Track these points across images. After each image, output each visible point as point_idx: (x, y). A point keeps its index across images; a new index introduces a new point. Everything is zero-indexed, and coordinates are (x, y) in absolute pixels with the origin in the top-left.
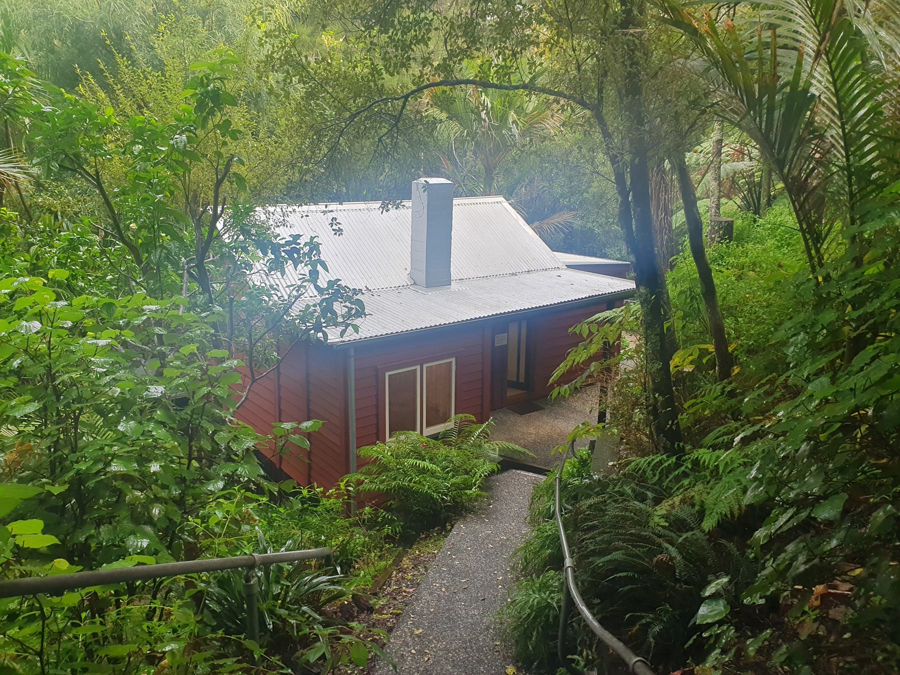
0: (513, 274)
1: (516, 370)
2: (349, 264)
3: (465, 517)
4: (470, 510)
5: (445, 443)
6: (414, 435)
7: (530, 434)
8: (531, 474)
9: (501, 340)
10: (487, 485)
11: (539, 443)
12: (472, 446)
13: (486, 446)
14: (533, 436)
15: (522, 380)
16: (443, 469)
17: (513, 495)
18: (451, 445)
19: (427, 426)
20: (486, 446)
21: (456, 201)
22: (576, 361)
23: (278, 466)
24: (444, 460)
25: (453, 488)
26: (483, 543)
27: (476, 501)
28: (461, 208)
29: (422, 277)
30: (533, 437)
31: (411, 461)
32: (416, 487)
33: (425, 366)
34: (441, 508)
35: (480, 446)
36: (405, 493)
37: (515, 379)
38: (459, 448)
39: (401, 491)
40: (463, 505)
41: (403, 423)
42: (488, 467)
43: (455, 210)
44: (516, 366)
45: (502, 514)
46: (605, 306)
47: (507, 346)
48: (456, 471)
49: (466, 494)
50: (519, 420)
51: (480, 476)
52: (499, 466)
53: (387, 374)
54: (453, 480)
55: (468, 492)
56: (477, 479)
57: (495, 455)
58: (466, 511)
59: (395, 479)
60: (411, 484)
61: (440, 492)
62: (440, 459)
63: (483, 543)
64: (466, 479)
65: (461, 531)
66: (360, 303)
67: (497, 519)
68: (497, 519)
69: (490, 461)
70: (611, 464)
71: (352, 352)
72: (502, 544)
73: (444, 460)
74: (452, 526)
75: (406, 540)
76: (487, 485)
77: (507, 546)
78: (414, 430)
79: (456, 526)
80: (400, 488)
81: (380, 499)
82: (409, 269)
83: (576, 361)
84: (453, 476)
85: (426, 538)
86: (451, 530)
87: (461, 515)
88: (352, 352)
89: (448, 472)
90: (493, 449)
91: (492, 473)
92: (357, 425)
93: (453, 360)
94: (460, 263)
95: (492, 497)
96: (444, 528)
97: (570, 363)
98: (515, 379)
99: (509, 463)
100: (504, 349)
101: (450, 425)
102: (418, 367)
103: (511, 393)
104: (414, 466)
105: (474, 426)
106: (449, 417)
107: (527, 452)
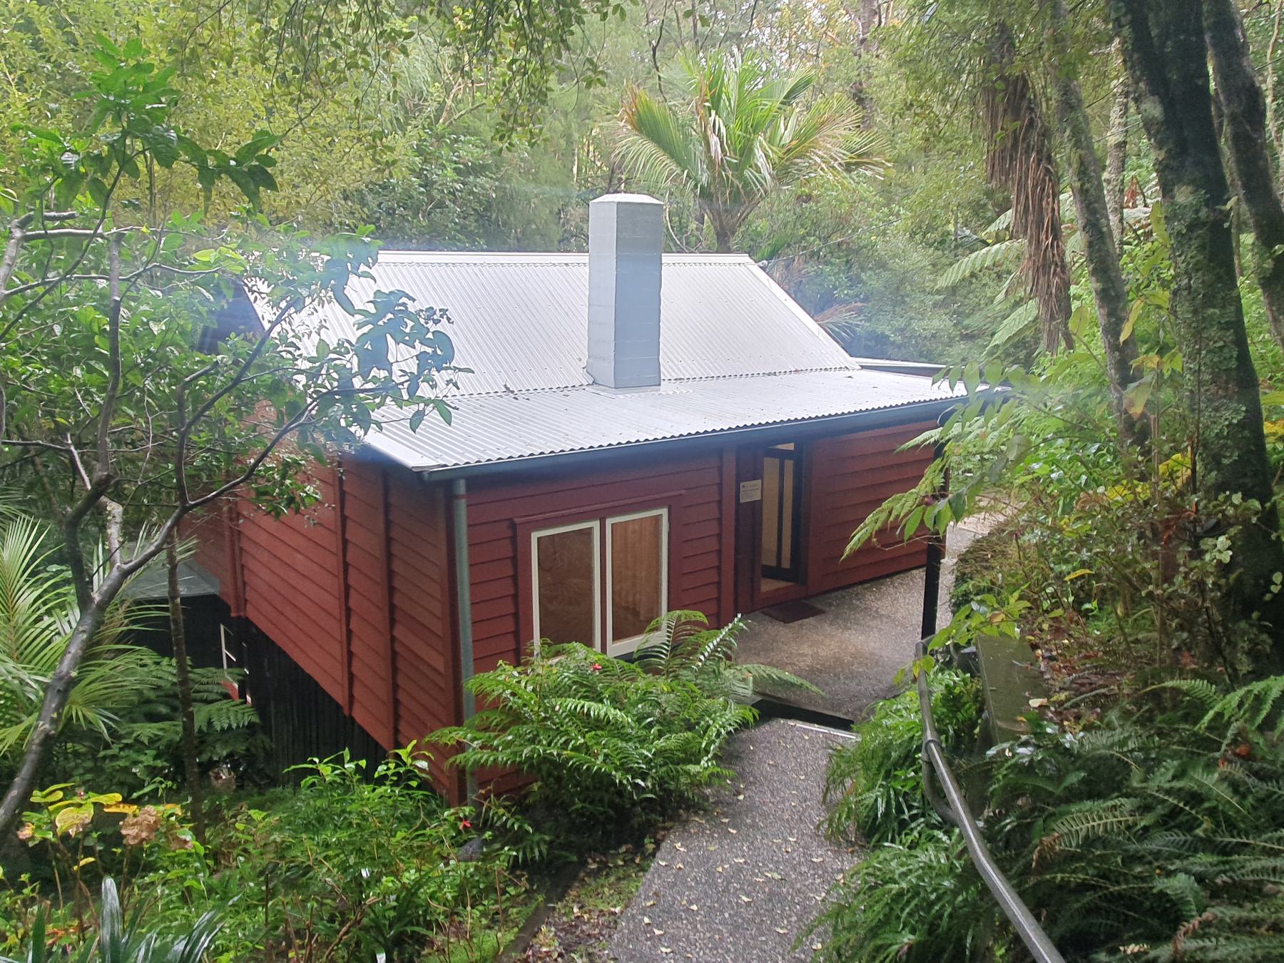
0: (769, 374)
1: (775, 549)
3: (687, 821)
4: (695, 807)
7: (803, 655)
8: (816, 727)
10: (729, 754)
11: (821, 671)
12: (701, 671)
13: (727, 673)
15: (786, 564)
16: (640, 719)
17: (784, 772)
20: (727, 673)
22: (894, 513)
25: (660, 760)
26: (726, 890)
27: (709, 785)
30: (809, 660)
31: (571, 703)
32: (573, 758)
34: (634, 804)
35: (717, 674)
36: (550, 769)
37: (773, 563)
39: (545, 767)
40: (681, 795)
41: (568, 626)
42: (734, 714)
43: (665, 271)
44: (783, 528)
45: (765, 816)
47: (760, 502)
48: (666, 725)
49: (687, 773)
50: (782, 631)
51: (718, 734)
52: (756, 712)
53: (535, 536)
54: (660, 743)
55: (693, 768)
56: (712, 739)
57: (747, 691)
58: (687, 809)
59: (533, 741)
61: (629, 770)
62: (634, 698)
63: (726, 890)
64: (687, 741)
65: (677, 853)
66: (442, 340)
67: (754, 826)
68: (754, 826)
69: (739, 702)
70: (1035, 703)
71: (461, 488)
72: (772, 893)
73: (641, 700)
74: (658, 844)
75: (553, 874)
76: (729, 754)
77: (782, 900)
78: (589, 643)
79: (665, 845)
80: (546, 759)
81: (511, 783)
82: (585, 360)
84: (660, 735)
85: (599, 870)
86: (653, 855)
87: (674, 817)
88: (461, 488)
89: (650, 725)
90: (743, 679)
91: (744, 725)
93: (664, 512)
94: (674, 353)
95: (742, 776)
96: (639, 846)
97: (883, 516)
99: (773, 706)
100: (756, 507)
101: (658, 639)
102: (595, 525)
103: (767, 586)
105: (705, 633)
106: (654, 612)
107: (806, 684)
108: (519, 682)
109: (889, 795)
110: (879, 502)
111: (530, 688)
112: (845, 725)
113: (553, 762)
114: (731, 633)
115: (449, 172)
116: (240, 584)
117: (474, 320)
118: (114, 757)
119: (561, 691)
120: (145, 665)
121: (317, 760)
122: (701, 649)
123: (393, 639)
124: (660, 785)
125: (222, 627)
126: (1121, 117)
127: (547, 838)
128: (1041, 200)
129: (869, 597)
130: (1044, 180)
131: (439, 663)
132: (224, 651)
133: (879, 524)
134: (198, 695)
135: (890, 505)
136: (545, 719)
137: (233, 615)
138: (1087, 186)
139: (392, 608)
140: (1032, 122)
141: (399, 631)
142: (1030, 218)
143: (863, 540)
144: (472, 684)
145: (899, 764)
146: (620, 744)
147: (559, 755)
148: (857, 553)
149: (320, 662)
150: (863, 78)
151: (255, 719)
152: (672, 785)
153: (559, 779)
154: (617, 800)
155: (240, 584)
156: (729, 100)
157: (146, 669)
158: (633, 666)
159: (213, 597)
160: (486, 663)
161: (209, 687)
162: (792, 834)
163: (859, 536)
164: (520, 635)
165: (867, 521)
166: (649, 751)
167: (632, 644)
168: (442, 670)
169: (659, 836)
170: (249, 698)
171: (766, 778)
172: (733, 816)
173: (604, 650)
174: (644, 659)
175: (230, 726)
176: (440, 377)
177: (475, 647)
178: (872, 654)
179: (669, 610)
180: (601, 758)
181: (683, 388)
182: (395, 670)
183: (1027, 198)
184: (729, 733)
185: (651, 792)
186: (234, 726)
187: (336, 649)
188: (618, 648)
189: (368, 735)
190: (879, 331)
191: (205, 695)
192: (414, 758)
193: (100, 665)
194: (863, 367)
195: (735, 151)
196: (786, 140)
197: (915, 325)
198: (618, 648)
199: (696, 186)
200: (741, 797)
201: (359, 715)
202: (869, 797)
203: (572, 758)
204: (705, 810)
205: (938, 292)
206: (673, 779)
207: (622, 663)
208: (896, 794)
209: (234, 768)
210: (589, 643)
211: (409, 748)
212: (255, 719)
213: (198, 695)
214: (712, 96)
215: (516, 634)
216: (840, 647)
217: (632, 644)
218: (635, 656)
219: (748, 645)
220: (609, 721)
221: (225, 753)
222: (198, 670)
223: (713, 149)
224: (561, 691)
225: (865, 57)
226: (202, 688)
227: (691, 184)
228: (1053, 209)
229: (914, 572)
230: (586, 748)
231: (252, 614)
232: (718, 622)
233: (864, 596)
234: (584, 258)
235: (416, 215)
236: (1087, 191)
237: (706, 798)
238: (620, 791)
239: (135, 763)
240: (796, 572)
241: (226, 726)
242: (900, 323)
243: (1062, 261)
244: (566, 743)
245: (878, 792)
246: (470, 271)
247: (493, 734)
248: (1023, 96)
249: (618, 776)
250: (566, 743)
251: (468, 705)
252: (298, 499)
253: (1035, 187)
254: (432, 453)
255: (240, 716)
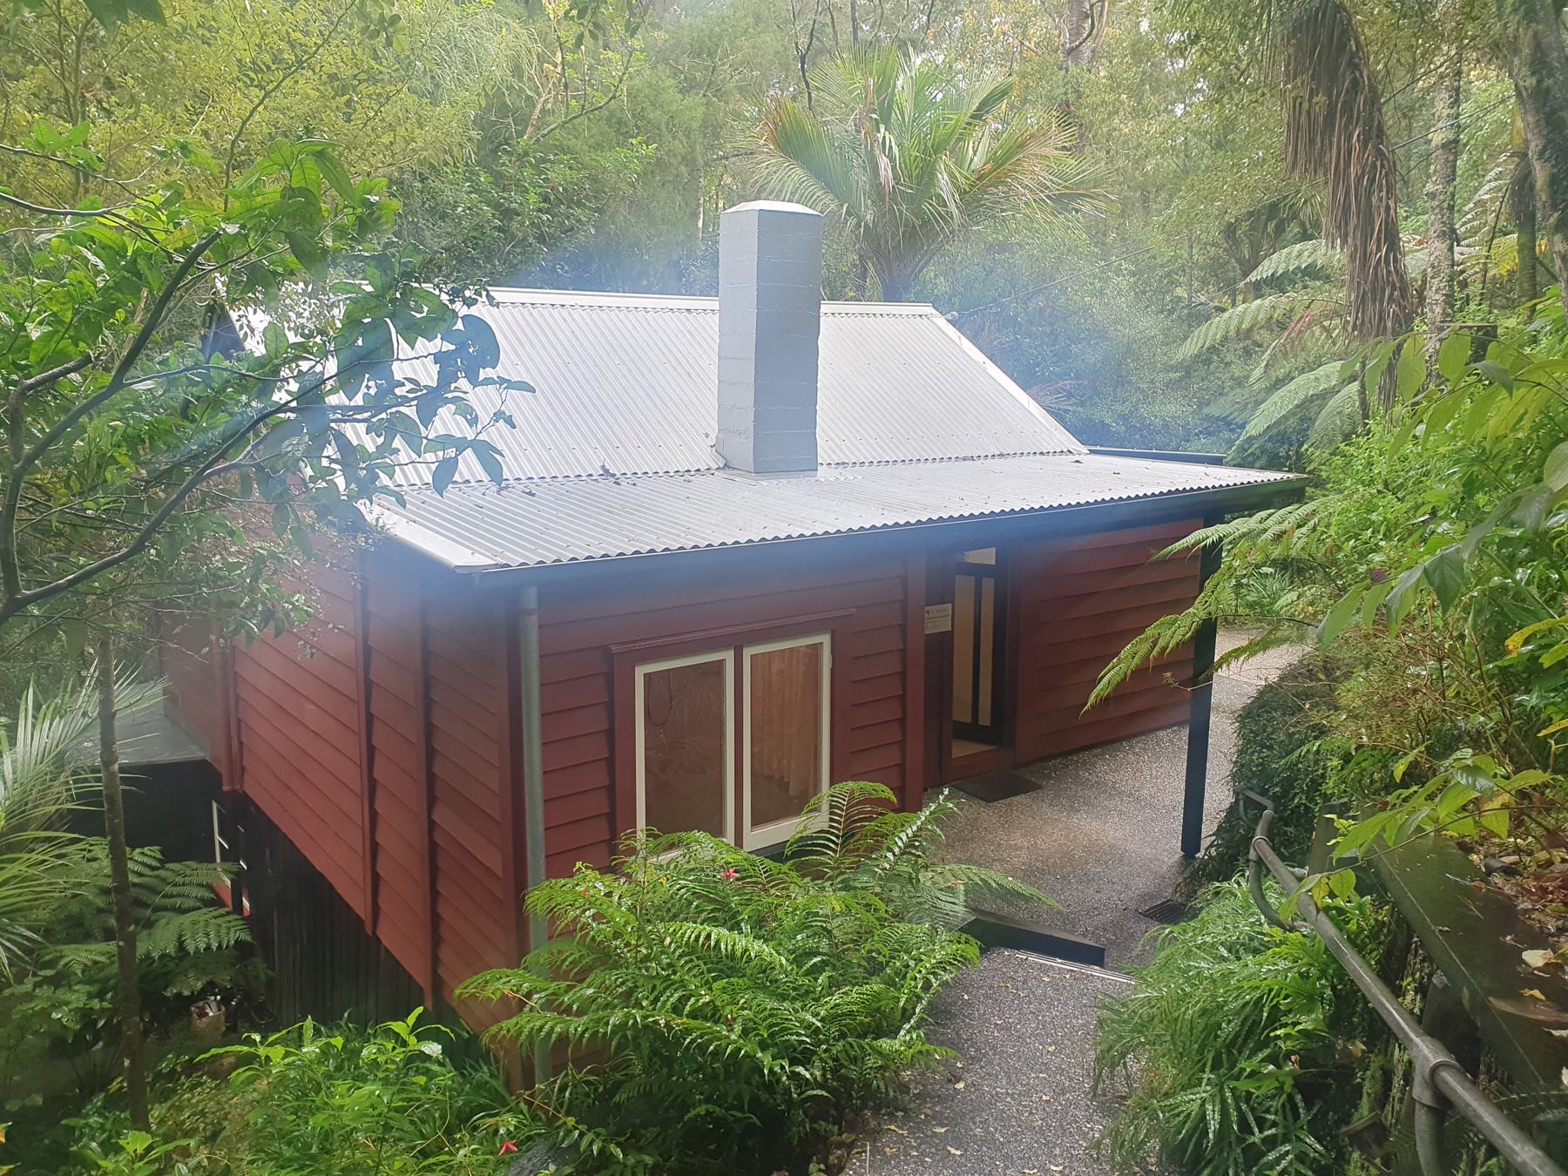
2: (565, 417)
5: (803, 871)
6: (703, 846)
8: (1057, 963)
9: (938, 620)
10: (941, 1015)
14: (1024, 854)
15: (985, 720)
16: (799, 957)
18: (820, 876)
19: (756, 823)
21: (825, 308)
22: (1161, 643)
23: (369, 930)
24: (803, 927)
27: (911, 1065)
28: (839, 323)
29: (744, 447)
31: (690, 930)
33: (748, 653)
37: (968, 719)
38: (847, 887)
41: (686, 806)
46: (1202, 521)
50: (987, 814)
51: (927, 986)
53: (640, 672)
55: (885, 1044)
57: (958, 909)
58: (876, 1110)
60: (679, 1022)
62: (788, 923)
64: (877, 996)
68: (988, 1140)
73: (803, 927)
78: (718, 831)
82: (713, 436)
83: (1161, 643)
84: (833, 985)
89: (815, 971)
90: (950, 887)
92: (547, 816)
93: (825, 640)
94: (835, 425)
97: (1144, 648)
98: (968, 719)
99: (995, 931)
100: (941, 646)
101: (814, 822)
102: (728, 656)
103: (961, 750)
104: (699, 952)
108: (609, 895)
109: (1223, 1101)
110: (1142, 630)
111: (627, 901)
112: (1094, 956)
113: (658, 1035)
114: (934, 819)
115: (533, 198)
116: (235, 743)
117: (560, 379)
118: (29, 997)
119: (673, 911)
120: (95, 859)
121: (257, 1037)
122: (889, 842)
123: (432, 825)
124: (834, 1071)
125: (215, 805)
126: (1451, 106)
127: (649, 1160)
128: (1369, 195)
129: (1102, 767)
130: (1374, 166)
131: (495, 861)
132: (218, 838)
133: (1136, 660)
134: (168, 902)
135: (1156, 632)
136: (647, 958)
137: (226, 788)
138: (1549, 82)
139: (431, 777)
140: (1355, 83)
141: (442, 815)
142: (1353, 221)
143: (1114, 683)
144: (537, 898)
145: (1235, 1046)
146: (771, 1004)
147: (667, 1024)
148: (1105, 701)
149: (336, 858)
150: (1072, 97)
151: (246, 937)
152: (853, 1072)
153: (669, 1062)
154: (764, 1096)
155: (235, 743)
156: (902, 114)
157: (95, 865)
158: (785, 868)
159: (202, 764)
160: (560, 866)
161: (186, 890)
162: (1052, 1157)
163: (1111, 675)
164: (616, 819)
165: (1122, 655)
166: (816, 1015)
167: (784, 830)
168: (499, 873)
169: (832, 1159)
170: (246, 903)
171: (994, 1048)
172: (951, 1122)
173: (739, 841)
174: (798, 855)
175: (208, 948)
176: (482, 399)
177: (547, 839)
178: (1112, 847)
179: (832, 783)
180: (738, 1028)
181: (848, 474)
182: (434, 871)
183: (1347, 195)
184: (944, 984)
185: (821, 1087)
186: (214, 946)
187: (356, 838)
188: (761, 837)
189: (398, 963)
190: (1097, 418)
191: (178, 902)
192: (420, 1038)
193: (14, 860)
194: (1092, 452)
195: (910, 177)
196: (978, 162)
197: (1143, 410)
198: (761, 837)
199: (858, 225)
200: (960, 1085)
201: (388, 936)
202: (1191, 1101)
203: (688, 1031)
204: (904, 1110)
205: (1174, 368)
206: (854, 1060)
207: (768, 862)
208: (1236, 1098)
209: (225, 1001)
210: (718, 831)
211: (411, 1019)
212: (246, 937)
213: (168, 902)
214: (881, 104)
215: (611, 817)
216: (1067, 837)
217: (784, 830)
218: (788, 852)
219: (959, 841)
220: (750, 960)
221: (199, 985)
222: (169, 865)
223: (882, 173)
224: (673, 911)
225: (1073, 70)
226: (176, 890)
227: (852, 222)
228: (1388, 208)
229: (1161, 733)
230: (712, 1013)
231: (252, 790)
232: (908, 803)
233: (1094, 765)
234: (714, 304)
235: (489, 259)
236: (1548, 91)
237: (904, 1088)
238: (771, 1085)
239: (56, 1006)
240: (999, 731)
241: (202, 946)
242: (1125, 409)
243: (1402, 279)
244: (683, 1000)
245: (1204, 1091)
246: (556, 314)
247: (563, 985)
248: (1342, 46)
249: (765, 1058)
250: (683, 1000)
251: (536, 931)
252: (280, 614)
253: (1359, 178)
254: (488, 549)
255: (224, 931)
